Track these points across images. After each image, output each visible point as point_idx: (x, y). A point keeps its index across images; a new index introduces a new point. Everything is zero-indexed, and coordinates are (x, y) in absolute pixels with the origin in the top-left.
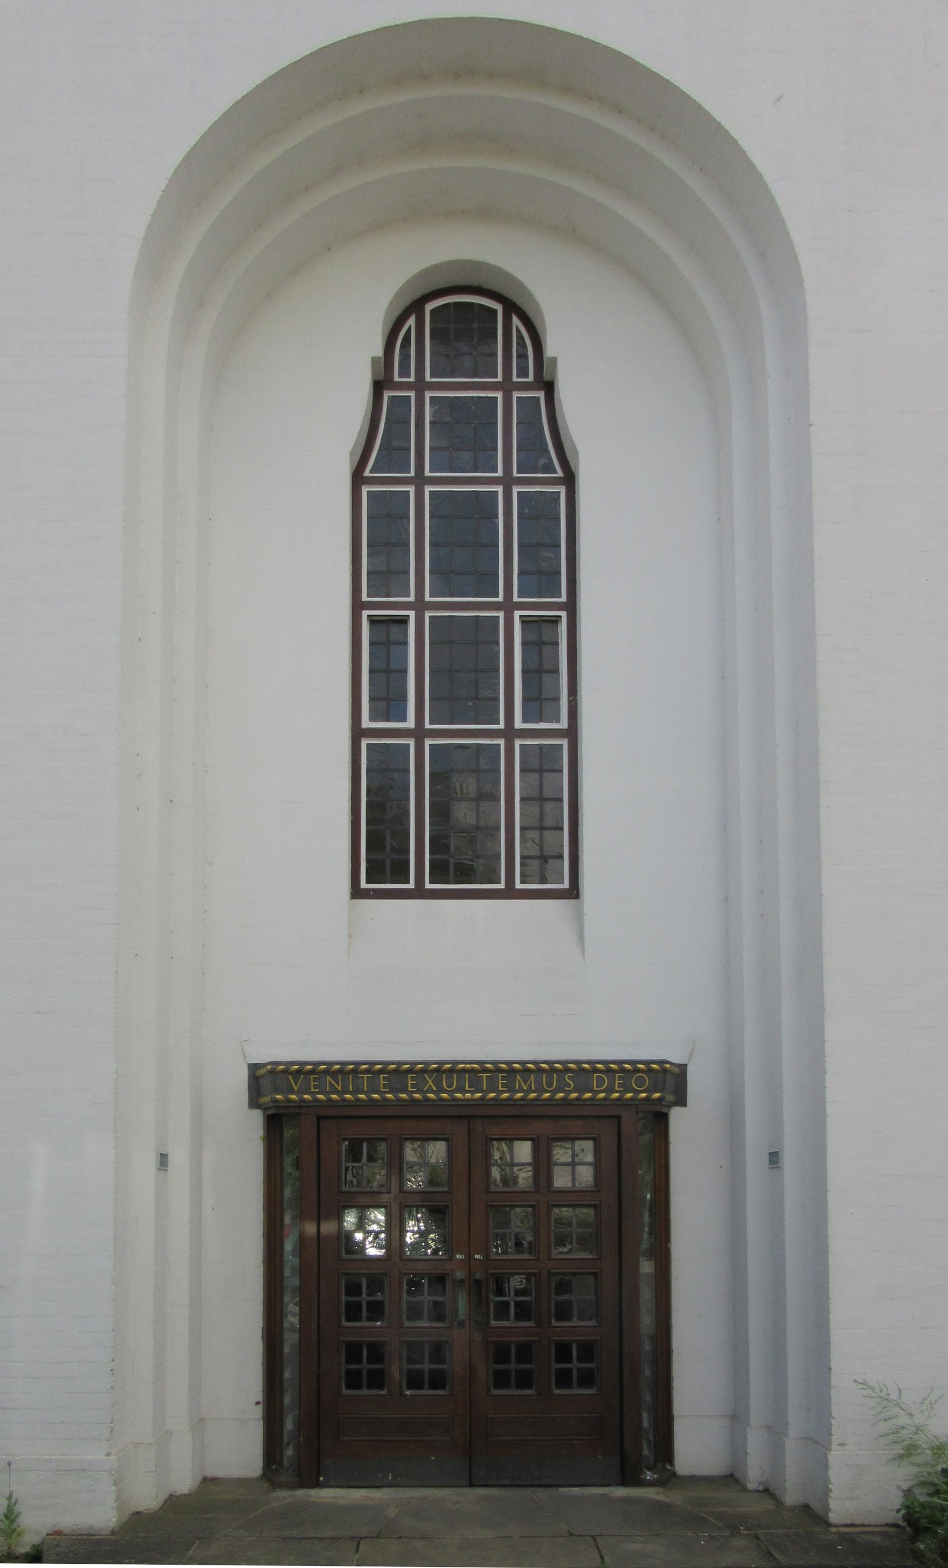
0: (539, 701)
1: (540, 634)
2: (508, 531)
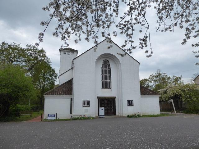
0: (109, 79)
1: (109, 76)
2: (108, 71)
